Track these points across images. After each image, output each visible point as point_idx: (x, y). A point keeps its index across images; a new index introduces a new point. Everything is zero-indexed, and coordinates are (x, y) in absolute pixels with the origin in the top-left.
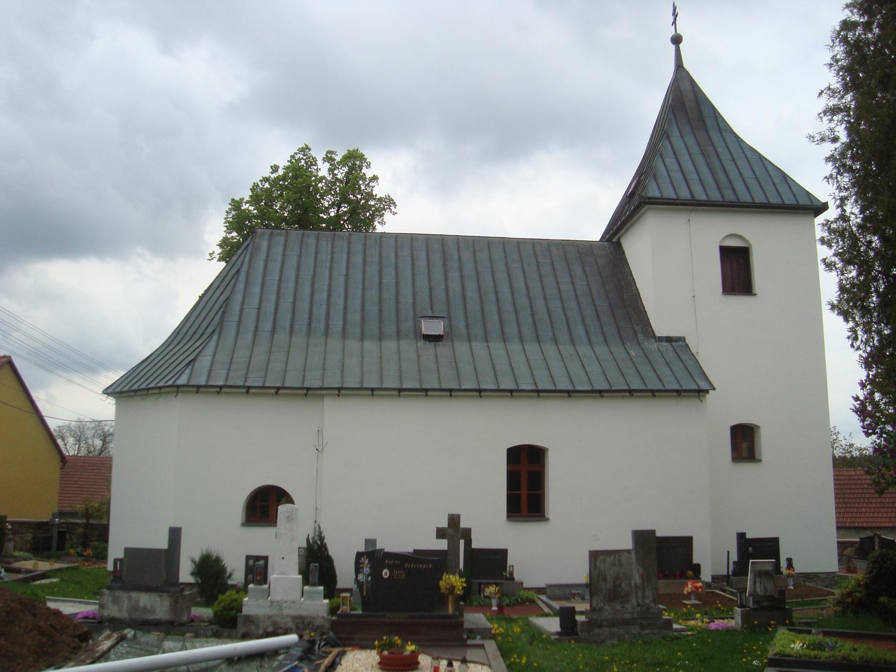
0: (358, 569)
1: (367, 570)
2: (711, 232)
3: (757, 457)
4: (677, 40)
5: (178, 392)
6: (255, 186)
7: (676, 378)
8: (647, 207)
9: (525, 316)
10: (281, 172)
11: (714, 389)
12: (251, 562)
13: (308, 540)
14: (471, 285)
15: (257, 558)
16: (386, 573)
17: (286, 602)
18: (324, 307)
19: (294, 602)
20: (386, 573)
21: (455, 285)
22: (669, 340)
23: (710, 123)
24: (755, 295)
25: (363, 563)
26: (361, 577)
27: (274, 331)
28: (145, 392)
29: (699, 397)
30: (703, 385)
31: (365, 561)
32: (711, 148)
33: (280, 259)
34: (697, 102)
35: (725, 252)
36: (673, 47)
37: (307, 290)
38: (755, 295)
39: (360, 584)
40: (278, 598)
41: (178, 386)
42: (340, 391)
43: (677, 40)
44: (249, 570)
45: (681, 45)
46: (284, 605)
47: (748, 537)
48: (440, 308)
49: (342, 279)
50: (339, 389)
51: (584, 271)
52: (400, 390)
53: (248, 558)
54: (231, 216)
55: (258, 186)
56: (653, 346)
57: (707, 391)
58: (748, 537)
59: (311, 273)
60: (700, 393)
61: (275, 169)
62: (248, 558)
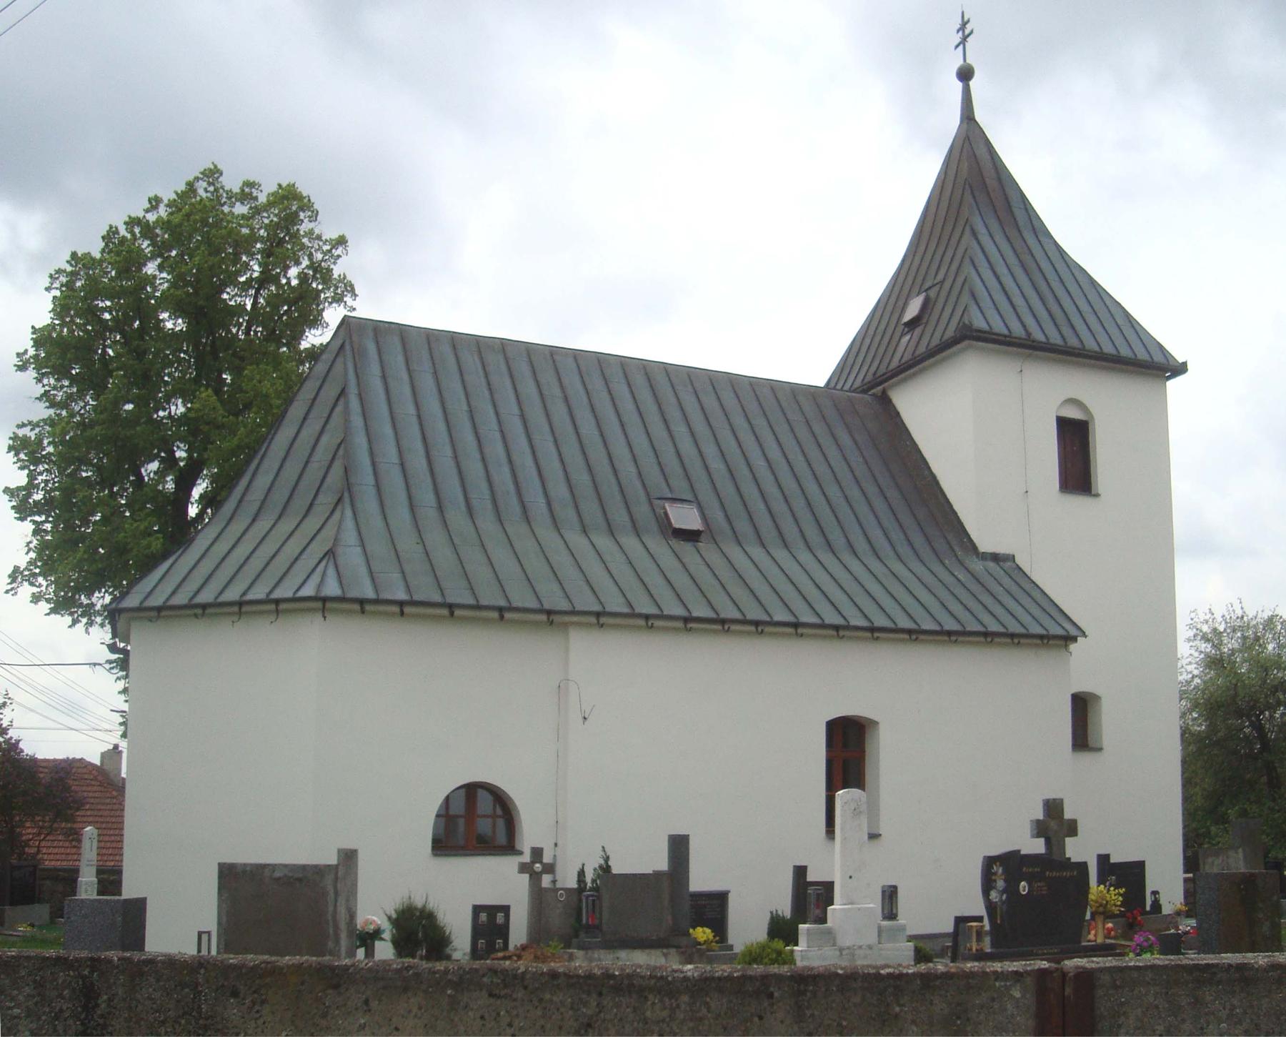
0: (988, 884)
1: (1000, 884)
2: (1048, 391)
3: (1091, 743)
4: (965, 74)
5: (277, 612)
6: (113, 231)
7: (1012, 618)
8: (966, 343)
9: (799, 504)
10: (163, 212)
11: (1084, 635)
12: (483, 917)
13: (581, 874)
14: (710, 450)
15: (492, 910)
16: (1024, 887)
17: (860, 947)
18: (506, 469)
19: (870, 947)
20: (1024, 887)
21: (687, 446)
22: (995, 558)
23: (1019, 214)
24: (1097, 495)
25: (995, 874)
26: (994, 895)
27: (440, 508)
28: (154, 614)
29: (1066, 646)
30: (1073, 632)
31: (998, 869)
32: (1029, 257)
33: (405, 376)
34: (1000, 180)
35: (1063, 423)
36: (960, 85)
37: (469, 438)
38: (1097, 495)
39: (990, 907)
40: (848, 944)
41: (277, 602)
42: (600, 618)
43: (965, 74)
44: (478, 931)
45: (971, 83)
46: (857, 952)
47: (1112, 861)
48: (681, 488)
49: (517, 423)
50: (598, 615)
51: (856, 442)
52: (686, 620)
53: (477, 910)
54: (57, 285)
55: (117, 232)
56: (977, 566)
57: (1074, 639)
58: (1112, 861)
59: (465, 408)
60: (1068, 639)
61: (155, 203)
62: (477, 910)
